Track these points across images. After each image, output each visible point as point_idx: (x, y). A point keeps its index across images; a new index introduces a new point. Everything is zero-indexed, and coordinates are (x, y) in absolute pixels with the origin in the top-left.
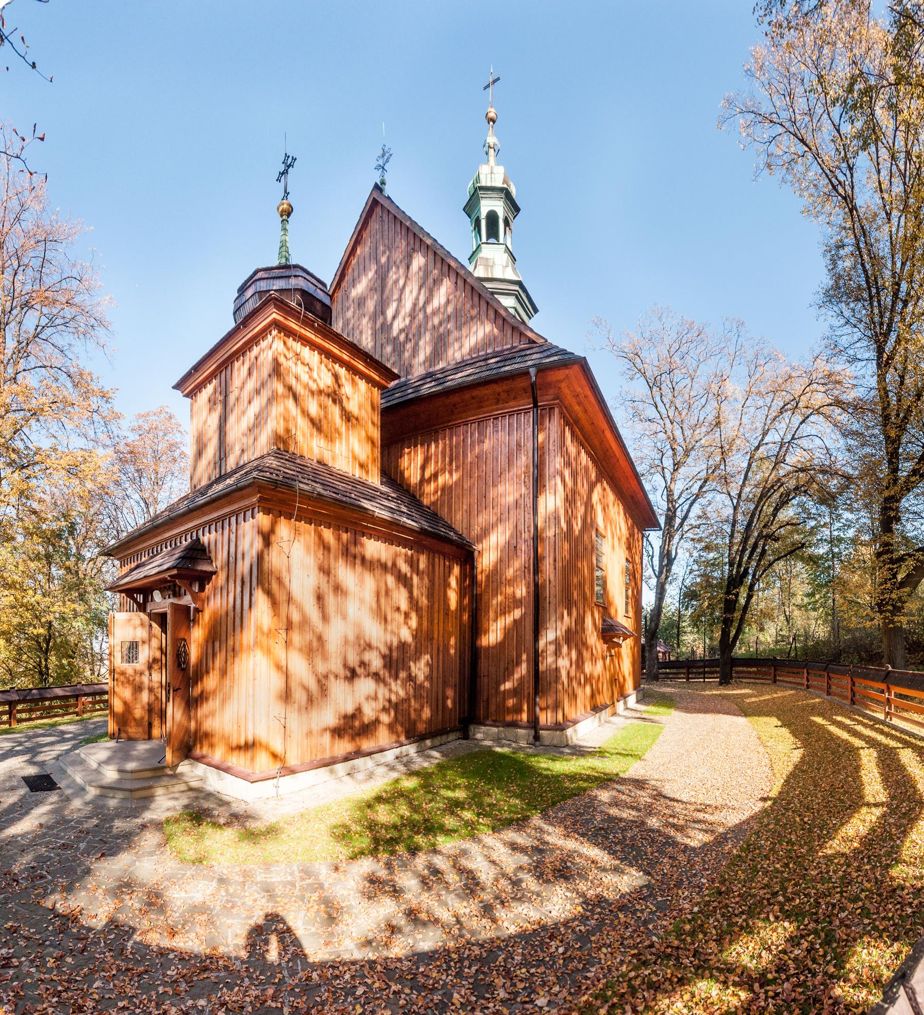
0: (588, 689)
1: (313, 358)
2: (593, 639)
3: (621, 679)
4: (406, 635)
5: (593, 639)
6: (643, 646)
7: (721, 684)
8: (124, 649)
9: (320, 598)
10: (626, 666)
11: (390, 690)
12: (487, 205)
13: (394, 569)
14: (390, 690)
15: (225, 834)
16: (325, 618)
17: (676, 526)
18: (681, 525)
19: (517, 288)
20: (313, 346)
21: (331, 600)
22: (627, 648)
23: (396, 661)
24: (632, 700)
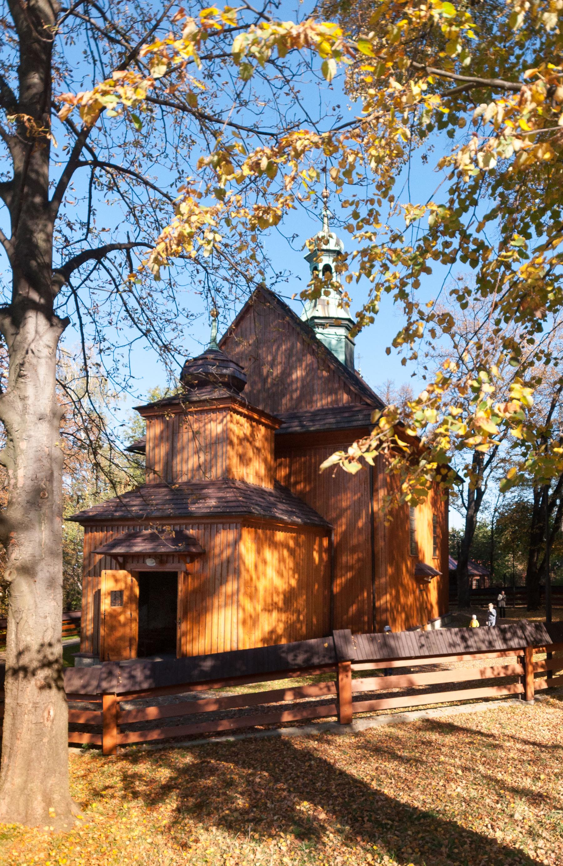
0: (403, 616)
1: (243, 420)
2: (407, 579)
3: (429, 606)
4: (293, 582)
5: (407, 579)
6: (452, 573)
7: (528, 609)
8: (106, 446)
9: (256, 567)
10: (433, 596)
11: (120, 97)
12: (327, 260)
13: (287, 547)
14: (120, 97)
15: (47, 402)
16: (258, 578)
17: (485, 463)
18: (489, 462)
19: (347, 322)
20: (245, 416)
21: (261, 567)
22: (433, 584)
23: (290, 597)
24: (438, 624)
